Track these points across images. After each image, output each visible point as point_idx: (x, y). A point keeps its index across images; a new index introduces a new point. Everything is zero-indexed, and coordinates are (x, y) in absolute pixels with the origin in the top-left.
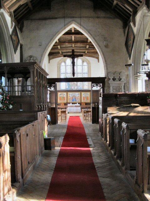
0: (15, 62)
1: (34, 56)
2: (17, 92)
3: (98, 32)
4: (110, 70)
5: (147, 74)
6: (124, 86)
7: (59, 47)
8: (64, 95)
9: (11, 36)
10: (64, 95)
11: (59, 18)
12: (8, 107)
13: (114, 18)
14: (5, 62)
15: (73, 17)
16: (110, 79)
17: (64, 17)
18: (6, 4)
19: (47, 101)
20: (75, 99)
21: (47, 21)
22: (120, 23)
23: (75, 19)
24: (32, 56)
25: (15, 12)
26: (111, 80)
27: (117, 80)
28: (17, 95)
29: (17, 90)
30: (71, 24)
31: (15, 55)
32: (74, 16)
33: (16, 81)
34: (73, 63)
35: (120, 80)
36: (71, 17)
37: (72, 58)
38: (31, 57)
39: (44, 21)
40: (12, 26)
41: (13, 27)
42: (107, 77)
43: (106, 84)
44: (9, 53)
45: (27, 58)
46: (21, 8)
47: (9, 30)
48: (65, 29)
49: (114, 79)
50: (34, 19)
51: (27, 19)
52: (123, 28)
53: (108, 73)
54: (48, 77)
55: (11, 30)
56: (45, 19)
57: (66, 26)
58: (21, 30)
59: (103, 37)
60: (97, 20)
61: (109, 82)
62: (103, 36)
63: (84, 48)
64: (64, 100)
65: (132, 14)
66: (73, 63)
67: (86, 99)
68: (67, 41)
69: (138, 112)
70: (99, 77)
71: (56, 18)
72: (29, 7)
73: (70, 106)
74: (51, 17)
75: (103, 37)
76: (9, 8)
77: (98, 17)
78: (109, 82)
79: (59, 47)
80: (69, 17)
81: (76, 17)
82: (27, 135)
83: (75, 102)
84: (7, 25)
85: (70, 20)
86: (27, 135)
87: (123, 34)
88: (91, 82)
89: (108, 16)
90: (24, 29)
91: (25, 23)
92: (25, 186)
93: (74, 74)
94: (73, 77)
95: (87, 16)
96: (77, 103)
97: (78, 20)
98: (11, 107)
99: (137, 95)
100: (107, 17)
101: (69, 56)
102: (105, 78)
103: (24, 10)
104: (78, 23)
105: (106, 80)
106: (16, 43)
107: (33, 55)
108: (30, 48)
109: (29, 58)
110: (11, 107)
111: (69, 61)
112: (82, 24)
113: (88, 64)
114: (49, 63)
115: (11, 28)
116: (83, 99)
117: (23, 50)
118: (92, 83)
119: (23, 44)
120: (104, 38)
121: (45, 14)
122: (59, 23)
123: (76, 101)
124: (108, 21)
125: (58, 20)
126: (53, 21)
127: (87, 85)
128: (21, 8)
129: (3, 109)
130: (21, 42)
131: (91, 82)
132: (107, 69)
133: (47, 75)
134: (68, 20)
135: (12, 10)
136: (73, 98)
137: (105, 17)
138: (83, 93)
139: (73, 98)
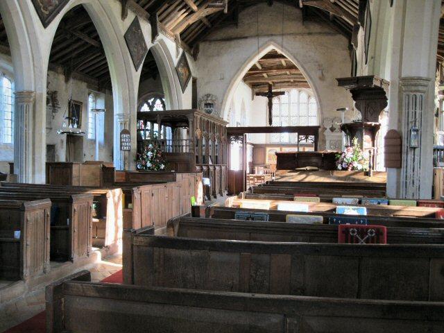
0: (184, 109)
2: (184, 148)
3: (310, 56)
4: (327, 115)
7: (265, 75)
9: (176, 69)
11: (251, 37)
12: (159, 167)
13: (335, 34)
14: (170, 109)
15: (272, 35)
17: (258, 36)
18: (167, 26)
21: (233, 43)
23: (275, 38)
25: (181, 34)
26: (328, 130)
28: (184, 151)
29: (184, 144)
30: (269, 45)
31: (183, 95)
32: (273, 33)
33: (162, 138)
34: (270, 105)
36: (268, 35)
37: (268, 97)
38: (208, 96)
39: (228, 43)
40: (177, 55)
41: (179, 56)
43: (320, 137)
44: (174, 92)
46: (192, 28)
47: (172, 61)
48: (258, 53)
49: (332, 129)
50: (214, 41)
51: (205, 41)
53: (323, 120)
54: (227, 126)
55: (176, 61)
56: (230, 39)
57: (266, 45)
58: (195, 57)
60: (308, 38)
61: (325, 133)
62: (317, 62)
66: (270, 105)
68: (275, 67)
69: (339, 178)
70: (305, 125)
71: (246, 38)
72: (204, 25)
74: (239, 36)
75: (317, 64)
76: (173, 30)
77: (310, 34)
78: (325, 133)
79: (265, 75)
80: (265, 35)
81: (275, 35)
82: (153, 195)
84: (171, 58)
85: (266, 39)
86: (153, 195)
88: (297, 134)
89: (326, 30)
90: (199, 55)
91: (202, 46)
93: (270, 121)
94: (268, 125)
95: (292, 32)
97: (279, 39)
98: (163, 166)
99: (296, 155)
100: (325, 33)
101: (264, 94)
102: (319, 127)
103: (197, 29)
104: (278, 44)
105: (320, 130)
106: (184, 78)
107: (213, 93)
108: (207, 83)
109: (205, 98)
110: (163, 166)
111: (265, 99)
112: (285, 44)
114: (253, 99)
115: (177, 57)
119: (198, 77)
120: (319, 65)
121: (231, 32)
122: (251, 44)
124: (325, 39)
125: (248, 41)
126: (242, 42)
128: (192, 28)
129: (153, 169)
130: (193, 74)
131: (297, 134)
132: (322, 113)
134: (263, 40)
135: (178, 33)
137: (320, 33)
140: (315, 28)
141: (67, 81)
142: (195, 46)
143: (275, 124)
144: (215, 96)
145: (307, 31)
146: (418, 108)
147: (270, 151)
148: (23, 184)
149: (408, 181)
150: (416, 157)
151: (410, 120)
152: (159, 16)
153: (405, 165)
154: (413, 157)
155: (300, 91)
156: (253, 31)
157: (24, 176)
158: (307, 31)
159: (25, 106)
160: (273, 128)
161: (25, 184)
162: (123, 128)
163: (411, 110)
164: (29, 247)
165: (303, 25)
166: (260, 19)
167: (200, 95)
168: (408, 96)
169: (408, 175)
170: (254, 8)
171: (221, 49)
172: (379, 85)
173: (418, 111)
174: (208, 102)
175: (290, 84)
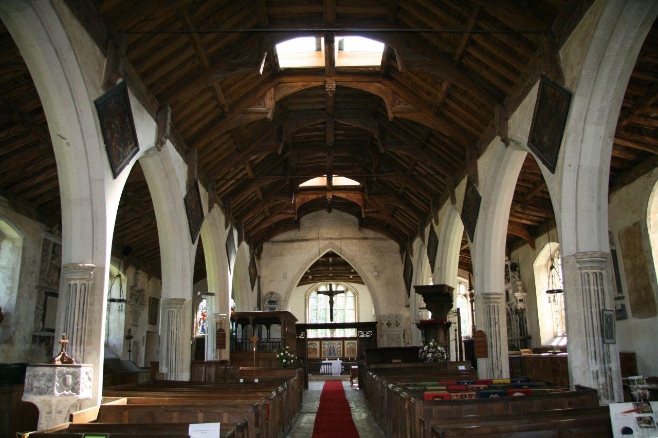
1: (276, 293)
5: (417, 324)
6: (404, 334)
8: (316, 345)
10: (316, 345)
16: (383, 324)
19: (394, 359)
20: (334, 351)
21: (295, 245)
22: (395, 246)
24: (273, 293)
27: (393, 325)
34: (331, 303)
35: (397, 326)
38: (272, 293)
39: (290, 245)
42: (379, 323)
45: (267, 295)
52: (400, 253)
54: (297, 323)
56: (292, 241)
59: (373, 265)
60: (364, 243)
62: (373, 264)
63: (347, 278)
64: (316, 353)
65: (419, 224)
66: (331, 303)
67: (352, 352)
71: (307, 240)
73: (326, 364)
75: (373, 265)
77: (365, 239)
83: (333, 356)
87: (400, 261)
89: (379, 235)
91: (266, 246)
92: (414, 173)
94: (331, 323)
96: (327, 359)
102: (376, 323)
105: (378, 325)
107: (274, 291)
113: (354, 294)
116: (348, 353)
117: (261, 284)
118: (358, 330)
121: (291, 234)
123: (335, 355)
126: (303, 244)
127: (351, 333)
133: (297, 320)
136: (330, 351)
137: (374, 238)
138: (346, 342)
139: (330, 351)
140: (370, 233)
141: (149, 279)
142: (259, 246)
143: (337, 320)
144: (279, 294)
145: (362, 235)
146: (496, 314)
147: (348, 344)
148: (168, 381)
149: (494, 367)
150: (498, 349)
151: (492, 323)
152: (244, 224)
153: (491, 355)
154: (496, 349)
155: (337, 285)
156: (313, 235)
157: (174, 374)
158: (362, 235)
159: (176, 312)
160: (335, 324)
161: (174, 381)
162: (219, 328)
163: (492, 316)
164: (451, 407)
165: (360, 230)
166: (319, 224)
167: (265, 292)
168: (489, 306)
169: (494, 363)
170: (314, 213)
171: (284, 249)
172: (448, 291)
173: (496, 317)
174: (272, 299)
175: (328, 278)
